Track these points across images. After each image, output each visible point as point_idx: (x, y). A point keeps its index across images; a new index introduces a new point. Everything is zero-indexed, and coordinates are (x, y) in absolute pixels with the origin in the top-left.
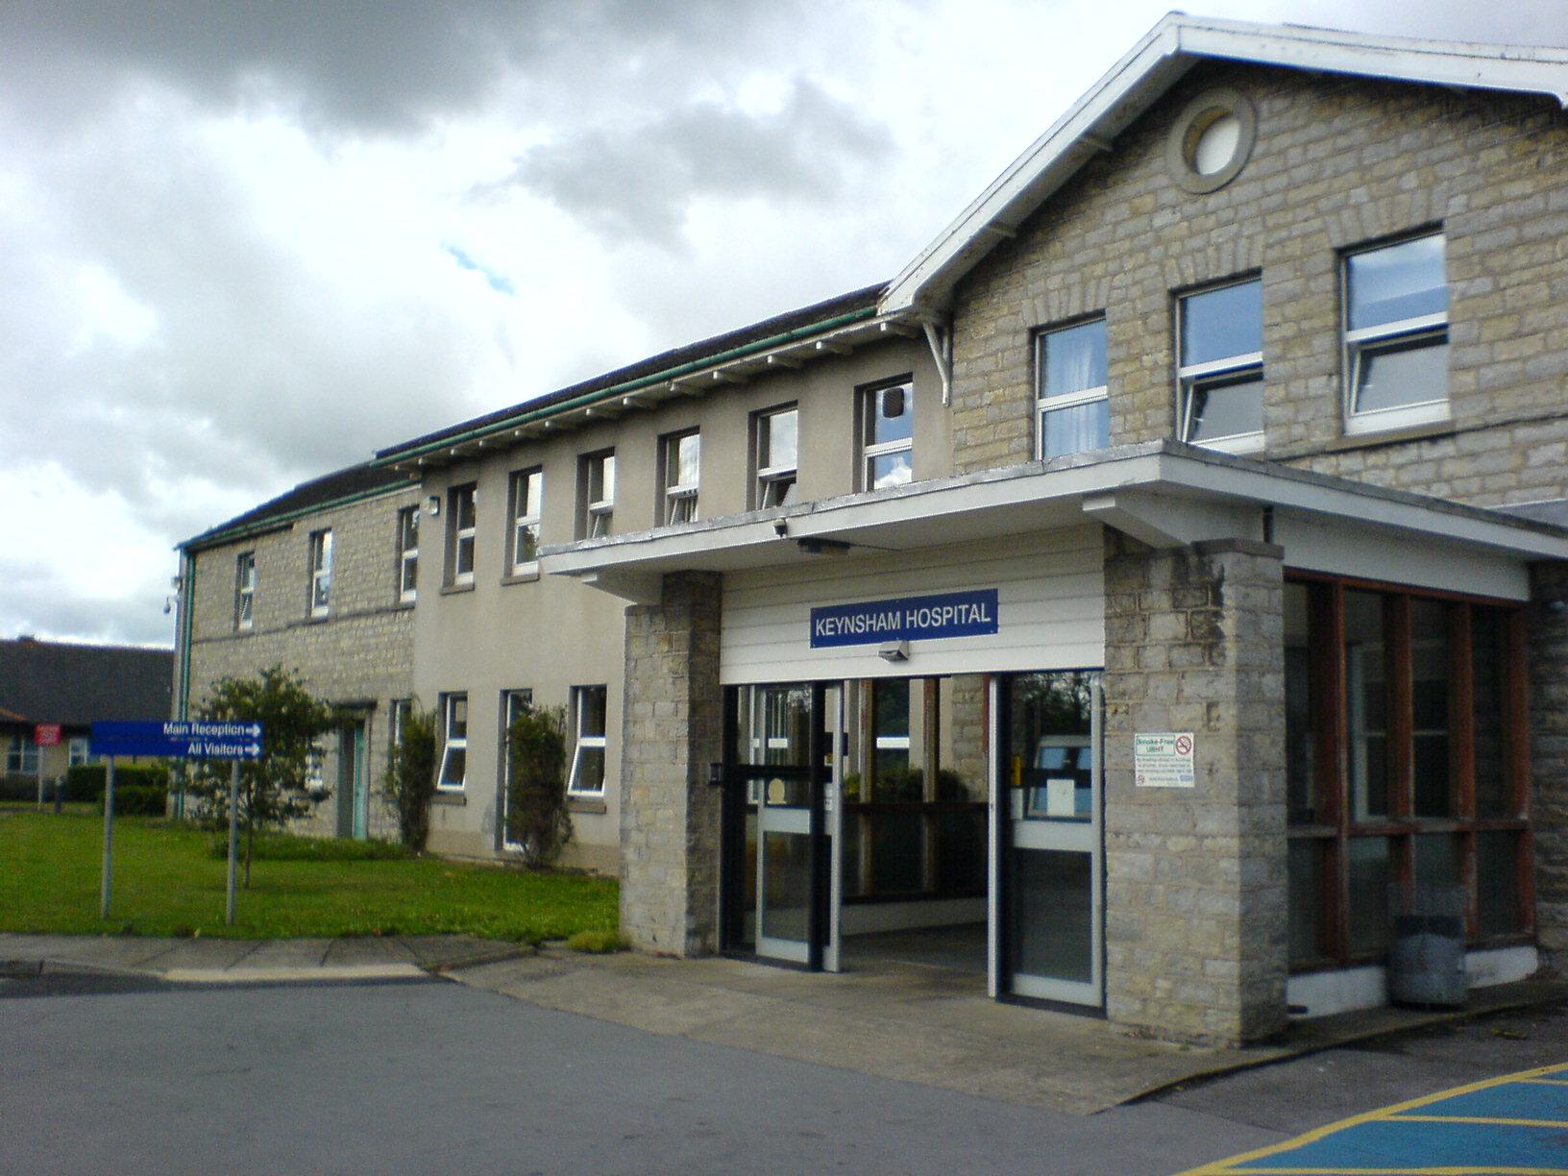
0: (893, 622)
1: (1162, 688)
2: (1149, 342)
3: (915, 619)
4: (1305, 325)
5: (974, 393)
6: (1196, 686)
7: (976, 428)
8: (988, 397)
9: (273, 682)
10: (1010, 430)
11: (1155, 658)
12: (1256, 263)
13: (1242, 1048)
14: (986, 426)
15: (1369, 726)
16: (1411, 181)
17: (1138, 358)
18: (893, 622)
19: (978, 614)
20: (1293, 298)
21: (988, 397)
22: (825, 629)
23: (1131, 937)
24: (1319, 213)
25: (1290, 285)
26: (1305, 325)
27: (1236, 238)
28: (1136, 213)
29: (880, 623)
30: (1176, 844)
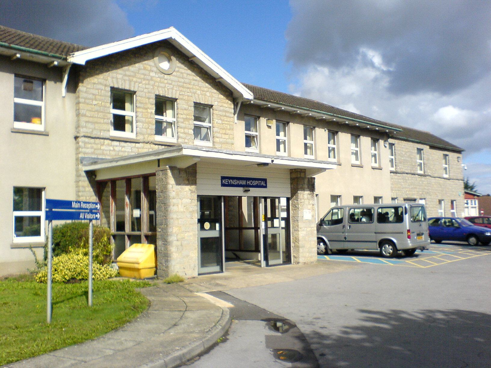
0: (244, 183)
1: (307, 202)
4: (188, 117)
5: (90, 99)
6: (311, 202)
7: (91, 111)
8: (95, 102)
10: (104, 116)
12: (177, 97)
14: (95, 111)
15: (46, 208)
16: (208, 94)
17: (146, 109)
18: (244, 183)
19: (263, 183)
20: (185, 109)
21: (95, 102)
22: (225, 182)
23: (303, 247)
24: (190, 92)
25: (185, 106)
26: (188, 117)
28: (145, 69)
30: (309, 229)
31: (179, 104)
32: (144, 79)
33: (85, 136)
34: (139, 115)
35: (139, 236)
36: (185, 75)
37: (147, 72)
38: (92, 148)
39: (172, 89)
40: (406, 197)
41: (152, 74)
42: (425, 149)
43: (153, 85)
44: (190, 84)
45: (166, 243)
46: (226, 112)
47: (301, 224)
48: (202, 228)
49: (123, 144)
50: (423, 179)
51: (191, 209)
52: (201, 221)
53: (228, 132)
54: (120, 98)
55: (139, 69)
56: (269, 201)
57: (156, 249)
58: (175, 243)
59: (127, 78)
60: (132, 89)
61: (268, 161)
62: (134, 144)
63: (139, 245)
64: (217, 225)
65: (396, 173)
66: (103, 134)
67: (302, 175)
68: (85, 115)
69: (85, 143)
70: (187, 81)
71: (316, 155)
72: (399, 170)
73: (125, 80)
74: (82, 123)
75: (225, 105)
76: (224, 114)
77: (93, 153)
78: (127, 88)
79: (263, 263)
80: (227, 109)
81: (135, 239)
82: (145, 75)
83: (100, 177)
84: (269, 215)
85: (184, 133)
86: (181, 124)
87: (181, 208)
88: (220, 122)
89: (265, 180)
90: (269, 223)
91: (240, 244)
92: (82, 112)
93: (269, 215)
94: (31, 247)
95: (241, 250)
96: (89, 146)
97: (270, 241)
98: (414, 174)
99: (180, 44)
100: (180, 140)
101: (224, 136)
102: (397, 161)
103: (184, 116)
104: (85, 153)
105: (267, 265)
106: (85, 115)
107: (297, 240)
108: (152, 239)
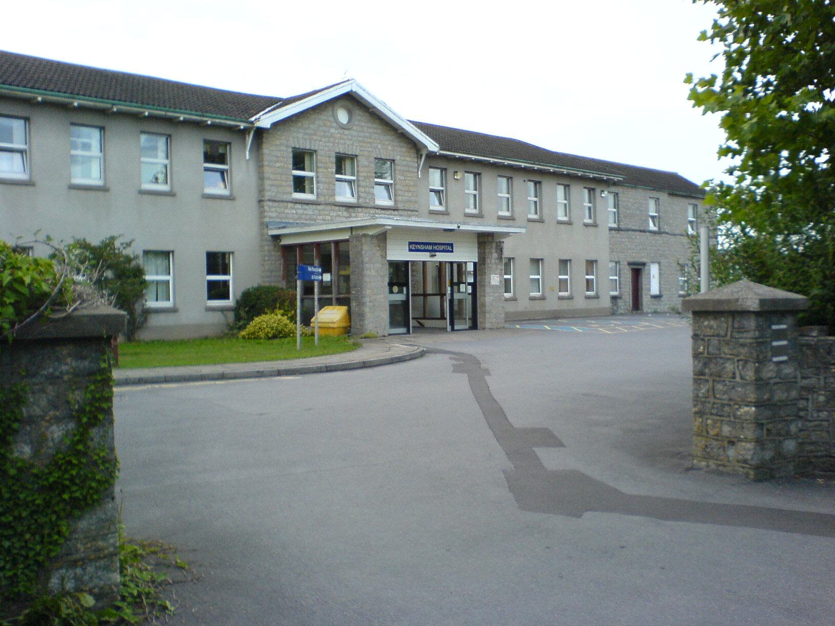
0: (430, 248)
1: (494, 266)
2: (330, 165)
3: (435, 248)
8: (278, 165)
9: (84, 240)
11: (493, 261)
13: (454, 371)
18: (430, 248)
21: (278, 165)
27: (353, 145)
28: (325, 125)
29: (428, 247)
31: (362, 161)
32: (324, 136)
33: (269, 200)
34: (320, 175)
35: (331, 299)
36: (365, 129)
37: (327, 129)
38: (276, 212)
39: (353, 145)
40: (631, 260)
41: (332, 130)
42: (661, 198)
43: (334, 143)
44: (370, 138)
45: (361, 304)
46: (408, 166)
47: (488, 290)
48: (391, 292)
49: (305, 207)
50: (658, 237)
51: (382, 274)
52: (391, 285)
53: (412, 189)
54: (299, 159)
55: (319, 126)
56: (455, 266)
57: (349, 312)
58: (368, 304)
59: (307, 137)
60: (313, 148)
61: (454, 227)
62: (315, 207)
63: (331, 307)
64: (405, 289)
65: (618, 230)
66: (285, 197)
67: (490, 239)
68: (269, 179)
69: (270, 207)
70: (367, 135)
71: (513, 211)
72: (622, 226)
73: (305, 139)
74: (267, 187)
75: (408, 159)
76: (407, 168)
77: (277, 217)
78: (308, 147)
79: (449, 328)
80: (411, 164)
81: (324, 303)
82: (325, 132)
83: (285, 242)
84: (455, 280)
85: (365, 192)
86: (362, 183)
87: (373, 273)
88: (402, 178)
89: (451, 245)
90: (456, 288)
91: (424, 312)
92: (266, 175)
93: (455, 280)
94: (222, 310)
95: (425, 318)
96: (273, 209)
97: (456, 308)
98: (644, 231)
99: (360, 96)
100: (360, 200)
101: (407, 194)
102: (621, 216)
103: (365, 174)
104: (271, 217)
105: (453, 329)
106: (269, 179)
107: (484, 305)
108: (341, 302)
